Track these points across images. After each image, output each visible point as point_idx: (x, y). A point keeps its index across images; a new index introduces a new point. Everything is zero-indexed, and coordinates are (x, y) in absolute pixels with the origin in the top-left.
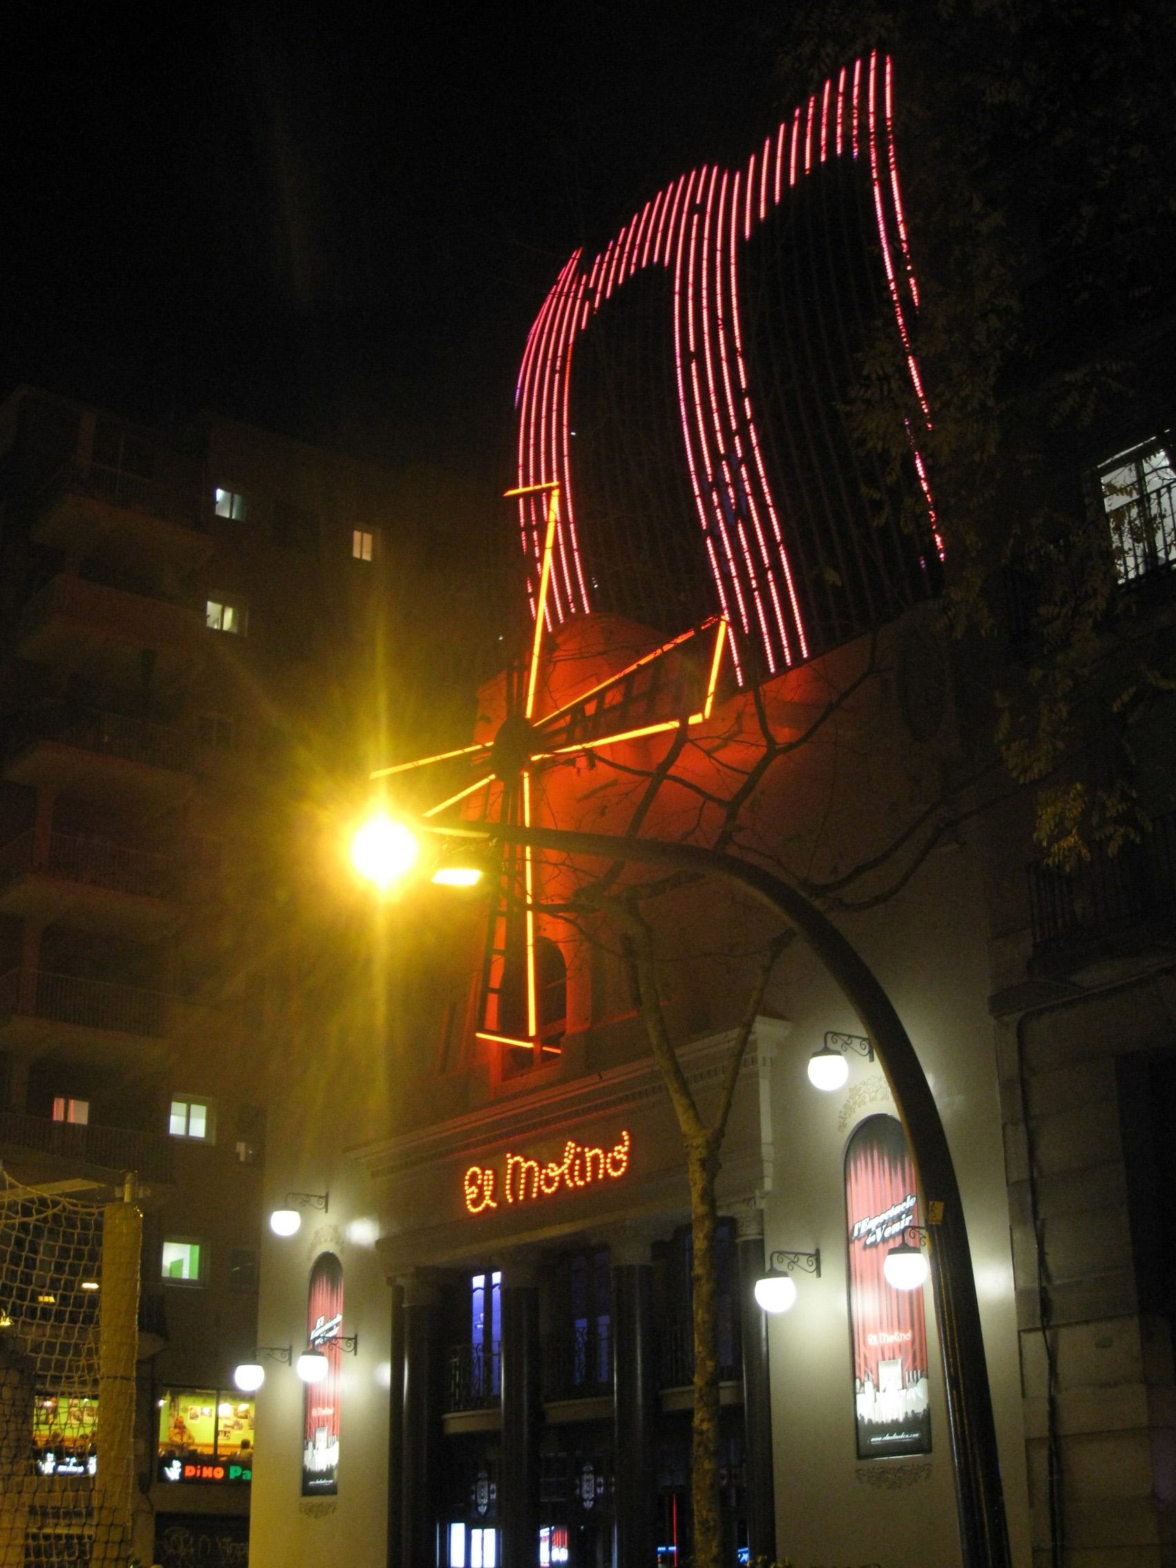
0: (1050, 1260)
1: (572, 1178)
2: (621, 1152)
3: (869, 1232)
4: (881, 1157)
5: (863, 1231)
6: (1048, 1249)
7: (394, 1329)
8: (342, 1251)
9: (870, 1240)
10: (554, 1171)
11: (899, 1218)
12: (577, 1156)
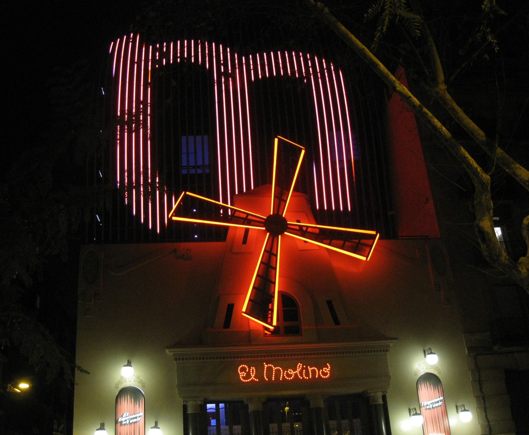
0: (488, 417)
1: (302, 375)
2: (327, 370)
3: (427, 405)
4: (430, 385)
5: (425, 405)
6: (488, 414)
7: (184, 420)
8: (439, 373)
9: (428, 407)
10: (291, 372)
11: (438, 402)
12: (303, 368)
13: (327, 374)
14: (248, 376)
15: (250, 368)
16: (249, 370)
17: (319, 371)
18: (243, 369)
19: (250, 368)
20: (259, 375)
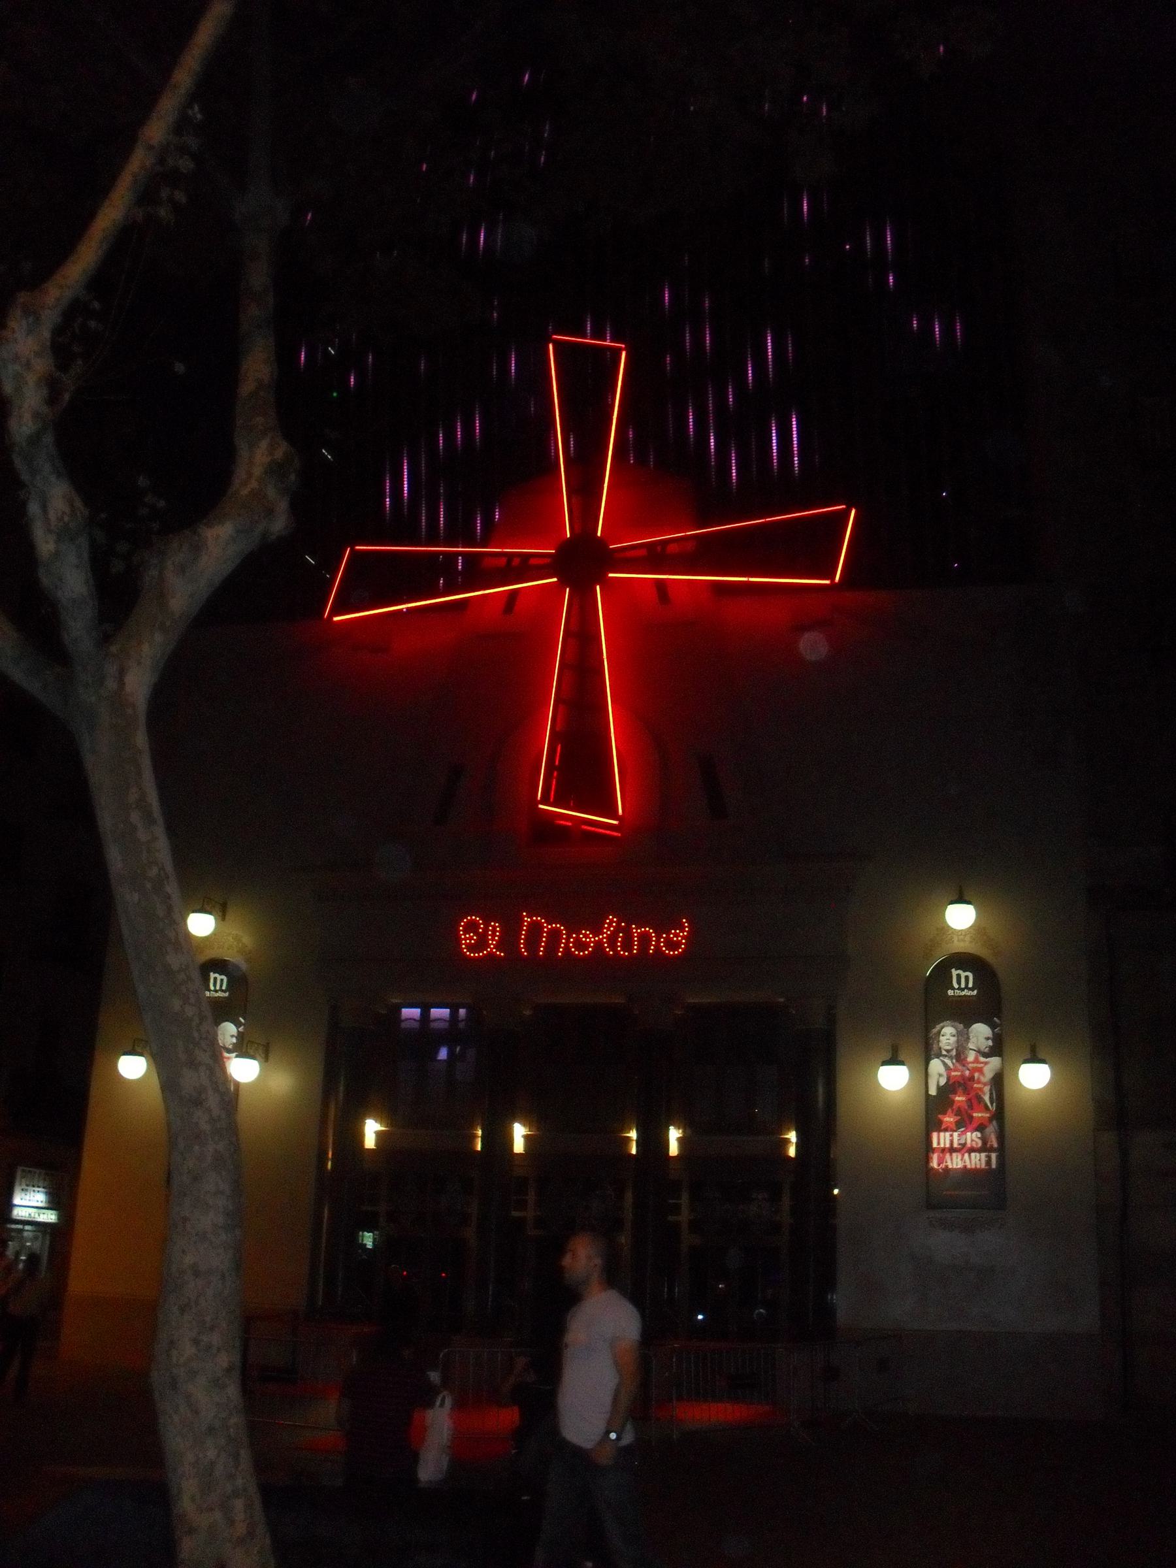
2: (680, 936)
13: (679, 944)
14: (482, 943)
15: (487, 925)
16: (486, 930)
17: (569, 936)
18: (472, 927)
19: (487, 925)
20: (508, 941)
